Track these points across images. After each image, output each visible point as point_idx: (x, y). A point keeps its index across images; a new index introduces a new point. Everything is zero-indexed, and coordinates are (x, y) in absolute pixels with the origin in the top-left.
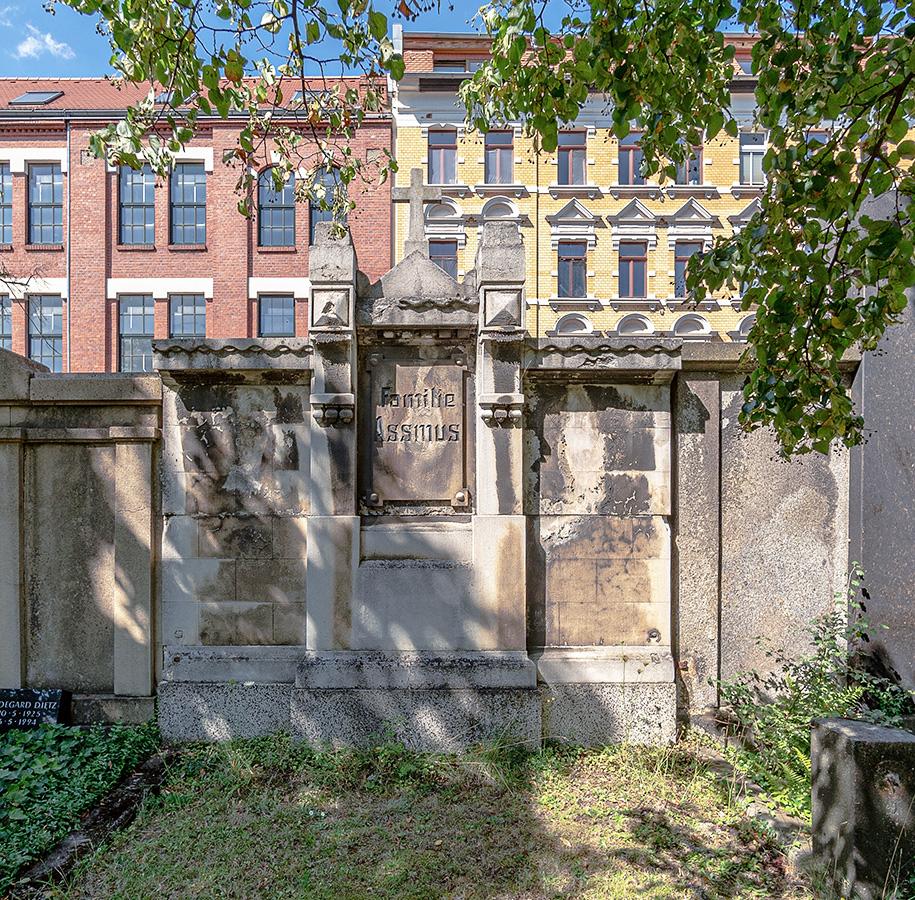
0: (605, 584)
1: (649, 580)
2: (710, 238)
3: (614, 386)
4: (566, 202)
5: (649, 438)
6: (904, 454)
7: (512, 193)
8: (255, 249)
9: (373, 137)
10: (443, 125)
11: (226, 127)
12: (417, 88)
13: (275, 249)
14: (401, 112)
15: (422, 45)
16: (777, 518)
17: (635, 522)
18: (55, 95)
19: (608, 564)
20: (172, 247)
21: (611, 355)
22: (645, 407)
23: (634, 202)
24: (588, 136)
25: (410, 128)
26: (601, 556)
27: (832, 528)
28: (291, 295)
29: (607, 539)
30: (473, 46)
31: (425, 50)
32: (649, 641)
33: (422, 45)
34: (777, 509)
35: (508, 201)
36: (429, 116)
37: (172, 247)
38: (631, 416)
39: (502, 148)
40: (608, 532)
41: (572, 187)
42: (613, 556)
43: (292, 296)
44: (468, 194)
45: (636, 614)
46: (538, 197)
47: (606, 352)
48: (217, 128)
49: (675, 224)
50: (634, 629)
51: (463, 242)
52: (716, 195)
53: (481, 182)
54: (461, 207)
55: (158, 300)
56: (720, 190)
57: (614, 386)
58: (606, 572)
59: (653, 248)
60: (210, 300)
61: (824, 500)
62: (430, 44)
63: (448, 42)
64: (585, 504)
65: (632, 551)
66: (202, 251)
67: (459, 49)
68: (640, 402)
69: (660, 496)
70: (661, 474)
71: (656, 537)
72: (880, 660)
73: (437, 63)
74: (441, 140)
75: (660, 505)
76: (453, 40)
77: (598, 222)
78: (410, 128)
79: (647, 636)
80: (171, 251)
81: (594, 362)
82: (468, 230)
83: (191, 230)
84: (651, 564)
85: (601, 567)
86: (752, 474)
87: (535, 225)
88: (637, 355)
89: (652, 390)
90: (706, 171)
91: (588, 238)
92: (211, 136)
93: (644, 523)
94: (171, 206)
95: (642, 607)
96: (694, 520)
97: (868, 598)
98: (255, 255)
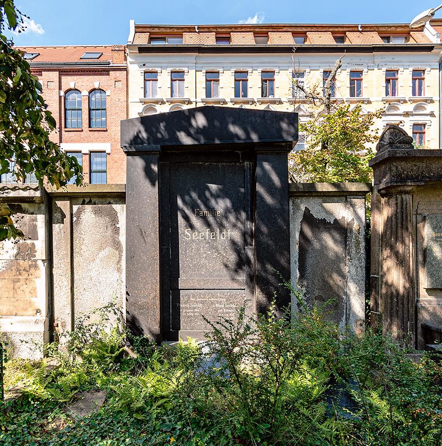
0: (18, 289)
1: (36, 288)
3: (20, 204)
5: (35, 227)
6: (144, 233)
7: (157, 102)
8: (63, 129)
10: (151, 69)
12: (137, 52)
13: (72, 130)
14: (131, 63)
15: (144, 30)
16: (98, 261)
17: (30, 263)
18: (35, 55)
19: (19, 280)
20: (90, 129)
21: (10, 190)
22: (33, 212)
24: (220, 74)
26: (15, 277)
27: (120, 265)
29: (18, 270)
30: (169, 30)
31: (146, 32)
32: (36, 314)
33: (144, 30)
34: (97, 257)
35: (155, 106)
36: (144, 65)
37: (90, 129)
38: (27, 217)
39: (179, 80)
40: (18, 267)
42: (20, 277)
43: (81, 152)
44: (163, 103)
45: (30, 302)
46: (196, 104)
47: (7, 189)
48: (44, 71)
50: (29, 309)
54: (403, 108)
57: (20, 204)
58: (18, 284)
61: (117, 253)
62: (148, 30)
63: (157, 29)
64: (8, 254)
65: (29, 275)
66: (105, 131)
67: (162, 32)
68: (31, 210)
69: (41, 251)
70: (41, 242)
71: (39, 269)
72: (135, 323)
74: (150, 76)
75: (40, 255)
76: (159, 27)
78: (136, 73)
79: (36, 312)
80: (90, 131)
81: (3, 194)
84: (36, 280)
85: (16, 282)
86: (86, 241)
88: (21, 191)
89: (37, 205)
90: (276, 91)
92: (108, 74)
93: (34, 263)
94: (90, 110)
95: (33, 299)
96: (60, 262)
97: (129, 295)
98: (63, 132)
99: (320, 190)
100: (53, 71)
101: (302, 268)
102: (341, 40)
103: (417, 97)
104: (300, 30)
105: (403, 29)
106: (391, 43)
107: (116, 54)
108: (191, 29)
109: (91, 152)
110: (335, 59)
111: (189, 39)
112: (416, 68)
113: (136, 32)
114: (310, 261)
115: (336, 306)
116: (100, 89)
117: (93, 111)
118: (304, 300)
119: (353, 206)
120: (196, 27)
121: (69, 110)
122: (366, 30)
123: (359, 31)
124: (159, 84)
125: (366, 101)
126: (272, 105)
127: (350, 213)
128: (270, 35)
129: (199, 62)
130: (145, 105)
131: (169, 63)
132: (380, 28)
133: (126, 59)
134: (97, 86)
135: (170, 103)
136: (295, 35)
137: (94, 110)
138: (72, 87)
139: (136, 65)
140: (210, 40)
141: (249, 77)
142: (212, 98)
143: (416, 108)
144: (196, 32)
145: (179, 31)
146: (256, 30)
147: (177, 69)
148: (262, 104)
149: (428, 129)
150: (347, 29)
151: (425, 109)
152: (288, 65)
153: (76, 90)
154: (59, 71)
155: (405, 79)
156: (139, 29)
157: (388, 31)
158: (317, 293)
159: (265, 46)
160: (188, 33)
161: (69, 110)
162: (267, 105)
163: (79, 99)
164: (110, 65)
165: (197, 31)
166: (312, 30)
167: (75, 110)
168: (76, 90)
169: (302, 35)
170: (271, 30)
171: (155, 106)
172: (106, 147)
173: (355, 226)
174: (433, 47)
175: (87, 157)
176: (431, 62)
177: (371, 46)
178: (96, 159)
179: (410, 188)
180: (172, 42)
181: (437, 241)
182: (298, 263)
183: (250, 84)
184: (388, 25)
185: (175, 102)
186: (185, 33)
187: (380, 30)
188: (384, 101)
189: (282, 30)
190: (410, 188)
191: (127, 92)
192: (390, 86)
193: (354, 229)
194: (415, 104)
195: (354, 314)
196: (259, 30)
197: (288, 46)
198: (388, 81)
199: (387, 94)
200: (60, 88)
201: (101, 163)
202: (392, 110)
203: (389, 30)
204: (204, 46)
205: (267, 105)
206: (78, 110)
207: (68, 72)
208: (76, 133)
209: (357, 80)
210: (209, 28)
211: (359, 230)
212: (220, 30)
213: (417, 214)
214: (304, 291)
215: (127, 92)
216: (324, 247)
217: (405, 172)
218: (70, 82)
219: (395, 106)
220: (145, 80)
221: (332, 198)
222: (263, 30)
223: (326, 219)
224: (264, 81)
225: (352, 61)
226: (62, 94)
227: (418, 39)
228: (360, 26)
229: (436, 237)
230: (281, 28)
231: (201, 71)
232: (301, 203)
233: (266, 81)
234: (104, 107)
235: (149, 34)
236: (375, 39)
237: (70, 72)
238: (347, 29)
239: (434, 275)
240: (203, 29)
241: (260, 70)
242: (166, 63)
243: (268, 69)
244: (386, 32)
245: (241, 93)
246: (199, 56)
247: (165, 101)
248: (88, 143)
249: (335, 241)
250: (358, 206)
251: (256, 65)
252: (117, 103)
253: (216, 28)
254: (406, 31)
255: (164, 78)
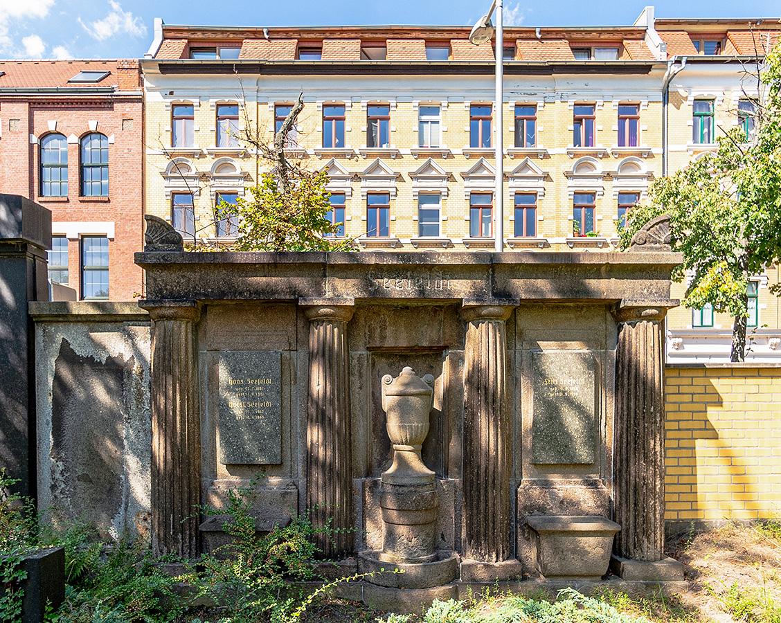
2: (646, 189)
4: (522, 161)
7: (192, 155)
9: (127, 110)
10: (182, 100)
11: (11, 102)
13: (51, 199)
14: (150, 90)
20: (81, 198)
23: (430, 161)
25: (157, 103)
28: (105, 236)
30: (220, 36)
31: (182, 39)
33: (179, 35)
35: (232, 161)
36: (171, 93)
41: (527, 149)
43: (65, 236)
48: (4, 102)
49: (514, 178)
51: (350, 194)
52: (399, 156)
53: (213, 146)
54: (601, 166)
55: (71, 240)
56: (402, 152)
59: (601, 197)
60: (112, 240)
62: (185, 34)
66: (105, 202)
67: (209, 39)
73: (705, 54)
74: (181, 111)
76: (203, 31)
77: (450, 177)
78: (157, 103)
82: (202, 184)
83: (97, 186)
87: (255, 180)
90: (392, 137)
91: (538, 190)
92: (112, 109)
94: (82, 168)
99: (74, 313)
100: (18, 102)
101: (58, 432)
102: (510, 52)
103: (627, 148)
104: (439, 36)
105: (611, 36)
106: (593, 59)
107: (124, 76)
108: (256, 34)
109: (83, 236)
110: (287, 88)
111: (252, 51)
112: (625, 100)
113: (165, 38)
114: (69, 421)
115: (110, 490)
116: (98, 133)
117: (87, 169)
118: (61, 481)
119: (130, 337)
120: (265, 30)
121: (48, 166)
122: (549, 36)
123: (536, 39)
124: (196, 124)
125: (541, 154)
126: (382, 160)
127: (128, 349)
128: (388, 44)
129: (264, 88)
130: (216, 159)
131: (214, 90)
132: (572, 33)
133: (141, 83)
134: (92, 128)
135: (213, 156)
136: (430, 44)
137: (89, 167)
138: (52, 128)
139: (159, 93)
140: (284, 52)
141: (347, 115)
142: (334, 148)
143: (624, 166)
144: (265, 39)
145: (235, 38)
146: (367, 36)
147: (227, 100)
148: (515, 158)
149: (600, 201)
150: (518, 36)
151: (639, 168)
152: (411, 94)
153: (59, 133)
154: (30, 103)
155: (606, 119)
156: (169, 33)
157: (588, 39)
158: (80, 470)
159: (369, 64)
160: (251, 41)
161: (48, 166)
162: (522, 160)
163: (64, 149)
164: (115, 93)
165: (267, 37)
166: (460, 36)
167: (57, 166)
168: (59, 134)
169: (444, 44)
170: (392, 36)
171: (232, 161)
172: (108, 228)
173: (136, 368)
174: (651, 66)
175: (77, 244)
176: (649, 90)
177: (547, 64)
178: (91, 249)
179: (172, 311)
180: (225, 55)
181: (236, 392)
182: (51, 424)
183: (348, 126)
184: (585, 29)
185: (222, 155)
186: (247, 41)
187: (573, 36)
188: (571, 154)
189: (409, 36)
190: (172, 311)
191: (143, 137)
192: (583, 129)
193: (134, 372)
194: (578, 159)
195: (136, 503)
196: (371, 36)
197: (467, 64)
198: (578, 121)
199: (577, 141)
200: (31, 131)
201: (101, 255)
202: (582, 170)
203: (588, 36)
204: (267, 63)
205: (522, 160)
206: (62, 166)
207: (44, 103)
208: (57, 204)
209: (483, 119)
210: (287, 32)
211: (141, 373)
212: (305, 36)
213: (289, 350)
214: (61, 468)
215: (143, 137)
216: (92, 400)
217: (168, 287)
218: (47, 120)
219: (589, 163)
220: (173, 118)
221: (103, 325)
222: (377, 36)
223: (95, 356)
224: (371, 121)
225: (519, 88)
226: (35, 140)
227: (634, 53)
228: (538, 30)
229: (235, 386)
230: (409, 32)
231: (266, 104)
232: (56, 332)
233: (375, 120)
234: (104, 163)
235: (360, 41)
236: (561, 52)
237: (49, 103)
238: (518, 36)
239: (231, 443)
240: (274, 34)
241: (364, 102)
242: (209, 90)
243: (378, 101)
244: (582, 42)
245: (335, 141)
246: (264, 80)
247: (206, 152)
248: (77, 223)
249: (109, 391)
250: (140, 337)
251: (359, 94)
252: (125, 156)
253: (299, 32)
254: (617, 39)
255: (205, 115)
